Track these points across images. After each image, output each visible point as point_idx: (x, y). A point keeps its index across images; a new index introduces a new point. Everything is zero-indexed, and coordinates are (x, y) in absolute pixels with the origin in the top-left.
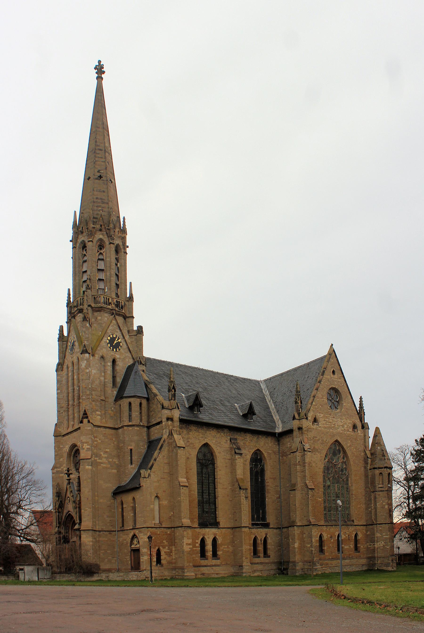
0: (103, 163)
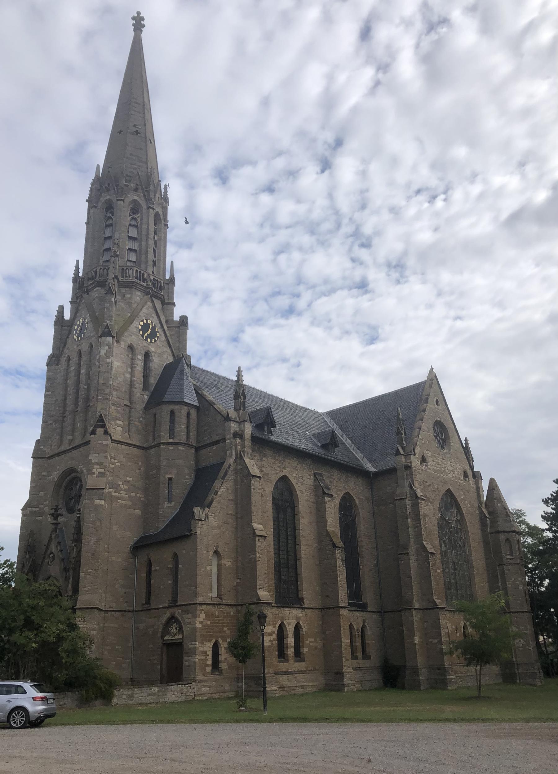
0: (141, 119)
